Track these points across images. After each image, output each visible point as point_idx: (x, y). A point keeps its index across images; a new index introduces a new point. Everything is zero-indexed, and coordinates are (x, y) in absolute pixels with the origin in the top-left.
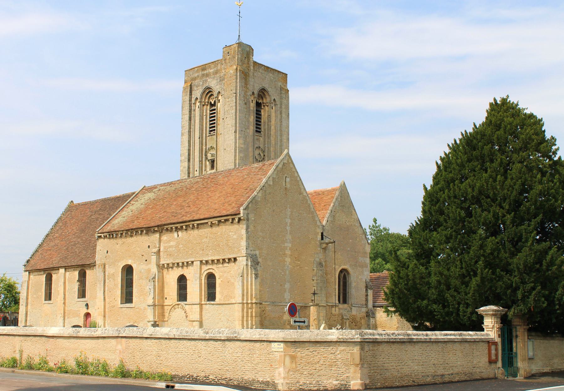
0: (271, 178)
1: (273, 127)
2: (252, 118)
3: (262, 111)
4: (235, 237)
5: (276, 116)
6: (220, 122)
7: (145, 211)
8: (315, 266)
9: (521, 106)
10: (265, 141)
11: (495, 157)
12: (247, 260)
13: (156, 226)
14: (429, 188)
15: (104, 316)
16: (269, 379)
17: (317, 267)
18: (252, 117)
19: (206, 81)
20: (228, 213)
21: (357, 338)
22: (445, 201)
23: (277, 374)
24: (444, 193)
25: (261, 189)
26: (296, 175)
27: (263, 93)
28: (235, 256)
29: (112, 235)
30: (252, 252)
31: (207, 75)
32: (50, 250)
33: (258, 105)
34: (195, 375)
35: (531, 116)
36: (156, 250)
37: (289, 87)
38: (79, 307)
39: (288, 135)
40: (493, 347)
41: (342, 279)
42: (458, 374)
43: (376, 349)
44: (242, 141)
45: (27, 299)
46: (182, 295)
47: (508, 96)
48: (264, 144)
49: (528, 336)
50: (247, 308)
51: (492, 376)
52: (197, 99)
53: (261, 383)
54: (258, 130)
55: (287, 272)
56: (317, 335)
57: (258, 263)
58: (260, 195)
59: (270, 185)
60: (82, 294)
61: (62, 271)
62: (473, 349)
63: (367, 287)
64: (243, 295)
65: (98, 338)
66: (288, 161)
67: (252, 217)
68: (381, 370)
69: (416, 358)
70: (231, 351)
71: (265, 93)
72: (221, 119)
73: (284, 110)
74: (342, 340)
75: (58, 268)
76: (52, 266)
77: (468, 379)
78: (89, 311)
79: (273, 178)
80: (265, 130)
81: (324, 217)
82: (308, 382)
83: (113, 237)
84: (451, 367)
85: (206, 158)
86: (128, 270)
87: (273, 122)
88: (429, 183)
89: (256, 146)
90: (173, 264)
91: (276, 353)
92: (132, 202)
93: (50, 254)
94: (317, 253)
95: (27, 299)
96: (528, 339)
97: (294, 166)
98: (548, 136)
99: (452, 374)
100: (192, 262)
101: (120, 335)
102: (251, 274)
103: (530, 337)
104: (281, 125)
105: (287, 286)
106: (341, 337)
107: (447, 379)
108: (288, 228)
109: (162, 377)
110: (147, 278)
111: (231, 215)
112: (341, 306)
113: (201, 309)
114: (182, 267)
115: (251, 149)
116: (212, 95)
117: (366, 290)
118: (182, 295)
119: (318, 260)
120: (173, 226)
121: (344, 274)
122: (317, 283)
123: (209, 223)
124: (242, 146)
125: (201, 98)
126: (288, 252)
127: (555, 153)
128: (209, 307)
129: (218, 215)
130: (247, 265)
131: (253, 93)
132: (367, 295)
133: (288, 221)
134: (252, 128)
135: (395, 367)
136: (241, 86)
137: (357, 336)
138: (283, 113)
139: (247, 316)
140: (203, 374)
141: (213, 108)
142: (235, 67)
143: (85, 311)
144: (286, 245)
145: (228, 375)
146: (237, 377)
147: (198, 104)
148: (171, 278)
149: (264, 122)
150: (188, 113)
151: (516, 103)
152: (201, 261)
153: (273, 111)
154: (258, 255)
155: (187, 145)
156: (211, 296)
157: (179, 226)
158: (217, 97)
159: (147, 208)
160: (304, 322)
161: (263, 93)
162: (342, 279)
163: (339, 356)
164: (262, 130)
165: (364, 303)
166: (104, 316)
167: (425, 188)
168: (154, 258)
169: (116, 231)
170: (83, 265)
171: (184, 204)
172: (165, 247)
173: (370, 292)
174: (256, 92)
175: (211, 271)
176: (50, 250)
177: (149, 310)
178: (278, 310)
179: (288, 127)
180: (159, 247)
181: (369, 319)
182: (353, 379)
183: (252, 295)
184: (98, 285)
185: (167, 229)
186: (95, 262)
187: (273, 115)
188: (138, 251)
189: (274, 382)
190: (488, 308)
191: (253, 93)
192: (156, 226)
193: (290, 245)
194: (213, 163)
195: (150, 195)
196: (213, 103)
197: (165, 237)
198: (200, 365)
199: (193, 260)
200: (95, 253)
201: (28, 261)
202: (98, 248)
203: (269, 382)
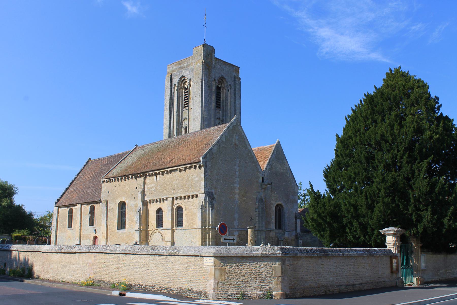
0: (224, 136)
1: (229, 104)
2: (214, 98)
3: (221, 93)
4: (197, 179)
5: (231, 97)
6: (191, 100)
7: (135, 163)
8: (257, 201)
9: (411, 74)
10: (223, 114)
11: (391, 119)
12: (205, 196)
13: (141, 173)
14: (340, 136)
15: (107, 239)
16: (201, 290)
17: (259, 202)
18: (214, 97)
19: (182, 71)
20: (192, 162)
21: (279, 254)
22: (354, 147)
23: (208, 285)
24: (352, 140)
25: (216, 144)
26: (243, 134)
27: (221, 80)
28: (196, 193)
29: (112, 179)
30: (209, 191)
31: (182, 68)
32: (73, 192)
33: (219, 89)
34: (144, 285)
35: (419, 81)
36: (141, 190)
37: (241, 76)
38: (88, 231)
39: (240, 110)
40: (394, 261)
41: (278, 211)
42: (366, 283)
43: (295, 263)
44: (206, 113)
45: (57, 226)
46: (159, 223)
47: (400, 67)
48: (223, 116)
49: (421, 252)
50: (206, 233)
51: (394, 284)
52: (175, 85)
53: (195, 293)
54: (218, 105)
55: (236, 206)
56: (244, 250)
57: (214, 198)
58: (215, 148)
59: (223, 141)
60: (92, 223)
61: (79, 206)
62: (379, 263)
63: (296, 218)
64: (202, 222)
65: (75, 253)
66: (237, 124)
67: (209, 164)
68: (301, 281)
69: (331, 270)
70: (172, 265)
71: (224, 80)
72: (192, 98)
73: (237, 92)
74: (265, 255)
75: (75, 205)
76: (72, 203)
77: (375, 288)
78: (96, 235)
79: (226, 136)
80: (223, 106)
81: (263, 165)
82: (235, 293)
83: (112, 181)
84: (361, 277)
85: (182, 127)
86: (122, 205)
87: (229, 101)
88: (341, 134)
89: (217, 117)
90: (154, 200)
91: (208, 267)
92: (128, 157)
93: (72, 195)
94: (259, 192)
95: (57, 226)
96: (421, 254)
97: (242, 128)
98: (433, 95)
99: (361, 284)
100: (167, 199)
101: (91, 251)
102: (209, 207)
103: (422, 253)
104: (235, 102)
105: (236, 216)
106: (264, 253)
107: (357, 288)
108: (237, 173)
109: (114, 286)
110: (135, 210)
111: (194, 163)
112: (277, 231)
113: (173, 231)
114: (160, 202)
115: (213, 119)
116: (186, 82)
117: (296, 220)
118: (159, 223)
119: (259, 197)
120: (154, 172)
121: (280, 208)
122: (259, 214)
123: (178, 169)
124: (206, 117)
125: (178, 84)
126: (237, 191)
127: (438, 109)
128: (178, 231)
129: (185, 163)
130: (205, 200)
131: (215, 80)
132: (296, 223)
133: (237, 168)
134: (213, 105)
135: (313, 279)
136: (206, 74)
137: (278, 252)
138: (236, 94)
139: (206, 238)
140: (150, 284)
141: (187, 91)
142: (201, 61)
143: (94, 235)
144: (235, 185)
145: (169, 285)
146: (176, 287)
147: (176, 88)
148: (153, 209)
149: (223, 101)
150: (169, 95)
151: (407, 72)
152: (173, 198)
153: (229, 93)
154: (214, 193)
155: (168, 117)
156: (180, 224)
157: (157, 172)
158: (189, 83)
159: (137, 161)
160: (234, 240)
161: (221, 80)
162: (278, 211)
163: (263, 270)
164: (222, 106)
165: (294, 229)
166: (107, 239)
167: (337, 136)
168: (140, 196)
169: (114, 177)
170: (93, 202)
171: (162, 157)
172: (148, 188)
173: (299, 221)
174: (216, 79)
175: (180, 205)
176: (73, 192)
177: (136, 234)
178: (220, 231)
179: (240, 104)
180: (144, 188)
181: (298, 241)
182: (275, 290)
183: (209, 222)
184: (103, 216)
185: (149, 175)
186: (101, 199)
187: (229, 95)
188: (125, 191)
189: (205, 292)
190: (389, 229)
191: (215, 80)
192: (141, 173)
193: (238, 186)
194: (186, 129)
195: (139, 152)
196: (186, 87)
197: (148, 179)
198: (148, 277)
199: (167, 197)
200: (101, 193)
201: (58, 200)
202: (103, 190)
203: (201, 292)
